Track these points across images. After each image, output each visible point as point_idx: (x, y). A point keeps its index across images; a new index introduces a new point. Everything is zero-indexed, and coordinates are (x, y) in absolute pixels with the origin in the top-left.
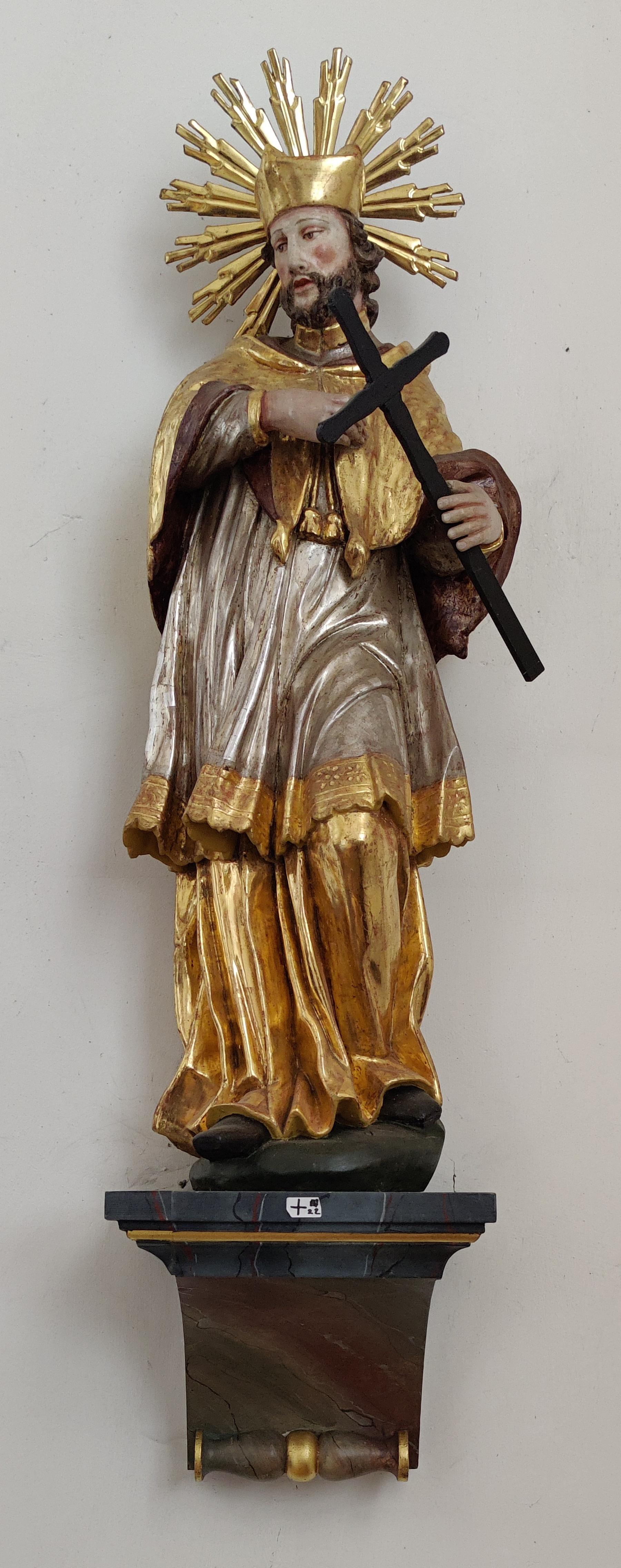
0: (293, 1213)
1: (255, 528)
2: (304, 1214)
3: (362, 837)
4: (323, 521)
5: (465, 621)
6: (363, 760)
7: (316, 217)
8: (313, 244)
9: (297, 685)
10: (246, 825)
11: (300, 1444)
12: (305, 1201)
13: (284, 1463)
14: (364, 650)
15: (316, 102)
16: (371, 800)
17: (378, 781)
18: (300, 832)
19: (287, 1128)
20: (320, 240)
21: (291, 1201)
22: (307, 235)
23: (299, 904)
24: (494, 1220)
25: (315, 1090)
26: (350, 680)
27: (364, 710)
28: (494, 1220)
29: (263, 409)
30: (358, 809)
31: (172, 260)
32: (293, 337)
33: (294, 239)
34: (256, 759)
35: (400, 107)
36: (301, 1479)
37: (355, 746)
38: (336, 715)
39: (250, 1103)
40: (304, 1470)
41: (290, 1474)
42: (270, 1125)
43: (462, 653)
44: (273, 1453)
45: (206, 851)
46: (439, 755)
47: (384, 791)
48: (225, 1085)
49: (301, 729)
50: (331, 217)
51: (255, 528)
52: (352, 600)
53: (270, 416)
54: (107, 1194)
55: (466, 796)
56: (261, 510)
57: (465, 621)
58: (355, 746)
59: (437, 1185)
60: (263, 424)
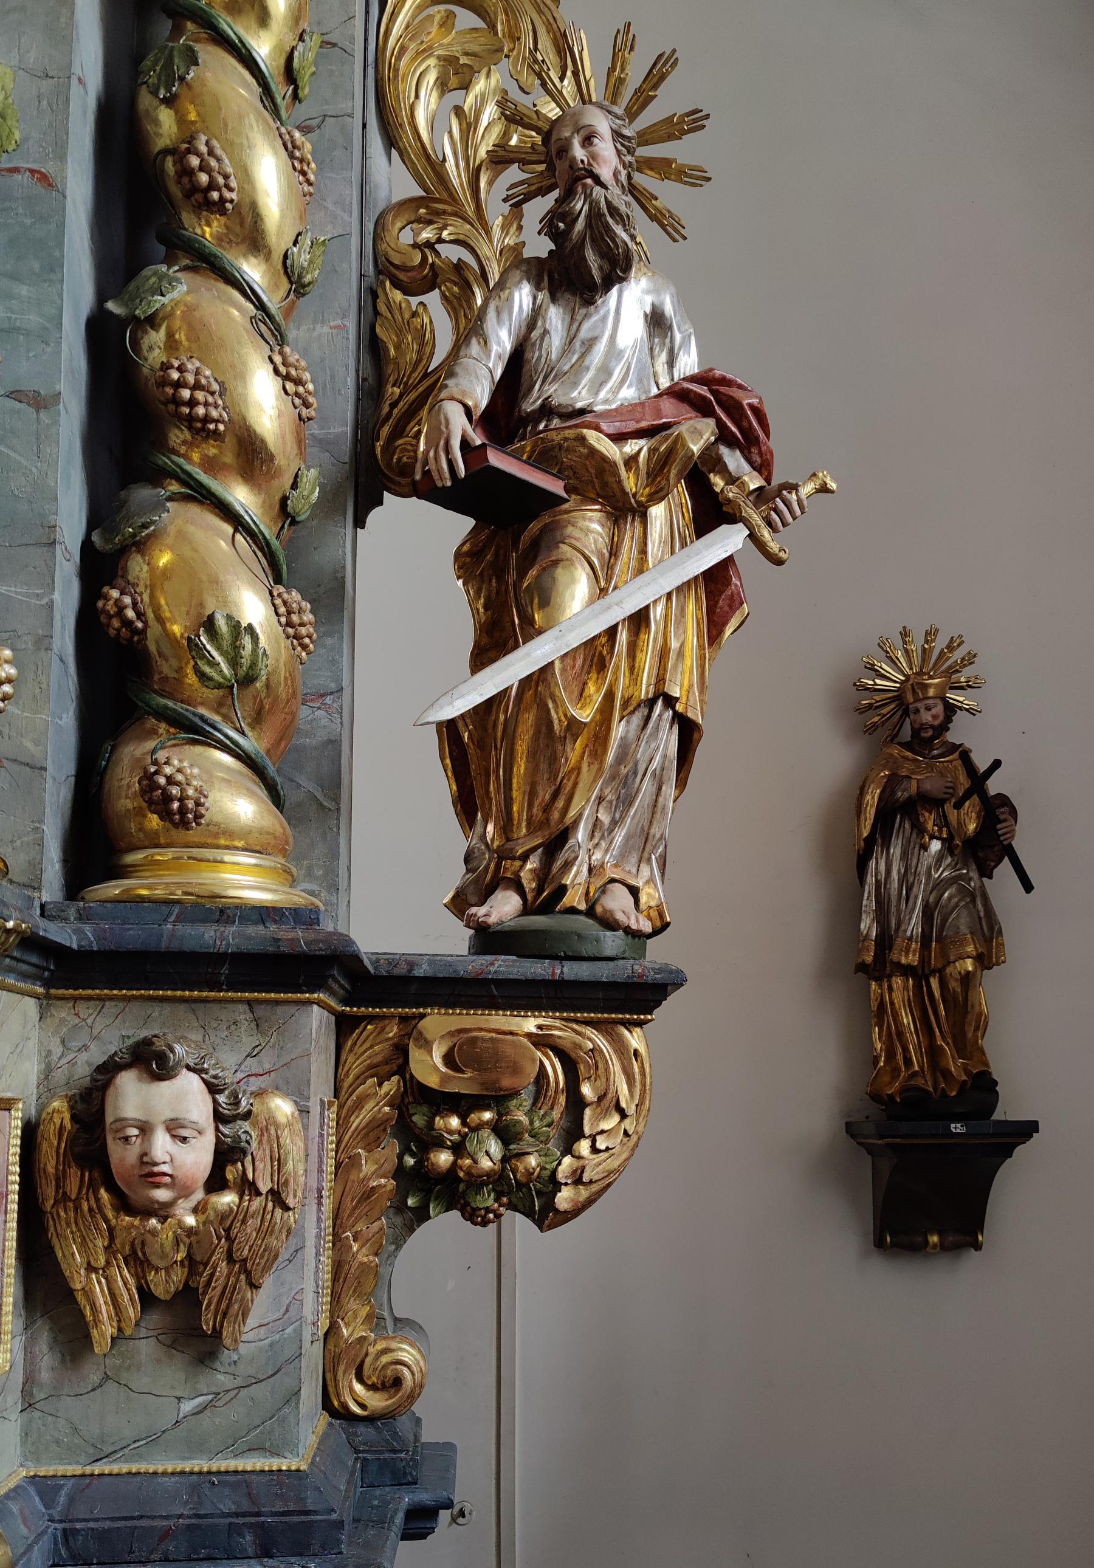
0: (954, 1130)
1: (911, 834)
2: (958, 1131)
3: (970, 969)
4: (940, 831)
5: (993, 864)
6: (969, 936)
7: (930, 702)
8: (930, 713)
9: (931, 899)
10: (916, 964)
11: (932, 1235)
12: (959, 1125)
13: (927, 1242)
14: (959, 884)
15: (923, 646)
16: (974, 953)
17: (978, 946)
18: (939, 965)
19: (938, 1094)
20: (934, 711)
21: (953, 1125)
22: (928, 709)
23: (937, 994)
24: (1038, 1132)
25: (947, 1074)
26: (956, 899)
27: (965, 913)
28: (1038, 1132)
29: (918, 787)
30: (969, 957)
31: (857, 710)
32: (201, 161)
33: (922, 711)
34: (917, 933)
35: (959, 645)
36: (933, 1251)
37: (964, 929)
38: (953, 916)
39: (919, 1081)
40: (935, 1246)
41: (928, 1249)
42: (930, 1091)
43: (990, 877)
44: (920, 1239)
45: (891, 971)
46: (991, 928)
47: (980, 950)
48: (903, 1074)
49: (937, 921)
50: (938, 701)
51: (911, 834)
52: (953, 863)
53: (921, 790)
54: (1037, 1122)
55: (1003, 944)
56: (913, 827)
57: (993, 864)
58: (964, 929)
59: (998, 1115)
60: (918, 793)
